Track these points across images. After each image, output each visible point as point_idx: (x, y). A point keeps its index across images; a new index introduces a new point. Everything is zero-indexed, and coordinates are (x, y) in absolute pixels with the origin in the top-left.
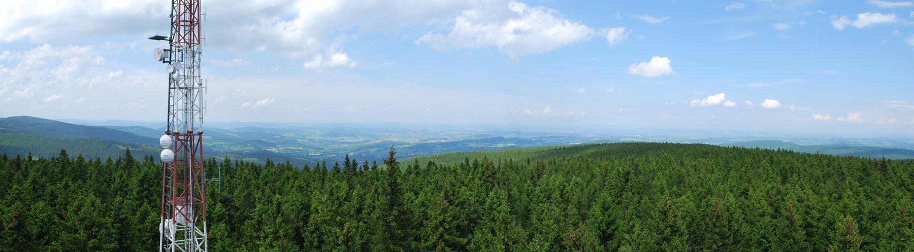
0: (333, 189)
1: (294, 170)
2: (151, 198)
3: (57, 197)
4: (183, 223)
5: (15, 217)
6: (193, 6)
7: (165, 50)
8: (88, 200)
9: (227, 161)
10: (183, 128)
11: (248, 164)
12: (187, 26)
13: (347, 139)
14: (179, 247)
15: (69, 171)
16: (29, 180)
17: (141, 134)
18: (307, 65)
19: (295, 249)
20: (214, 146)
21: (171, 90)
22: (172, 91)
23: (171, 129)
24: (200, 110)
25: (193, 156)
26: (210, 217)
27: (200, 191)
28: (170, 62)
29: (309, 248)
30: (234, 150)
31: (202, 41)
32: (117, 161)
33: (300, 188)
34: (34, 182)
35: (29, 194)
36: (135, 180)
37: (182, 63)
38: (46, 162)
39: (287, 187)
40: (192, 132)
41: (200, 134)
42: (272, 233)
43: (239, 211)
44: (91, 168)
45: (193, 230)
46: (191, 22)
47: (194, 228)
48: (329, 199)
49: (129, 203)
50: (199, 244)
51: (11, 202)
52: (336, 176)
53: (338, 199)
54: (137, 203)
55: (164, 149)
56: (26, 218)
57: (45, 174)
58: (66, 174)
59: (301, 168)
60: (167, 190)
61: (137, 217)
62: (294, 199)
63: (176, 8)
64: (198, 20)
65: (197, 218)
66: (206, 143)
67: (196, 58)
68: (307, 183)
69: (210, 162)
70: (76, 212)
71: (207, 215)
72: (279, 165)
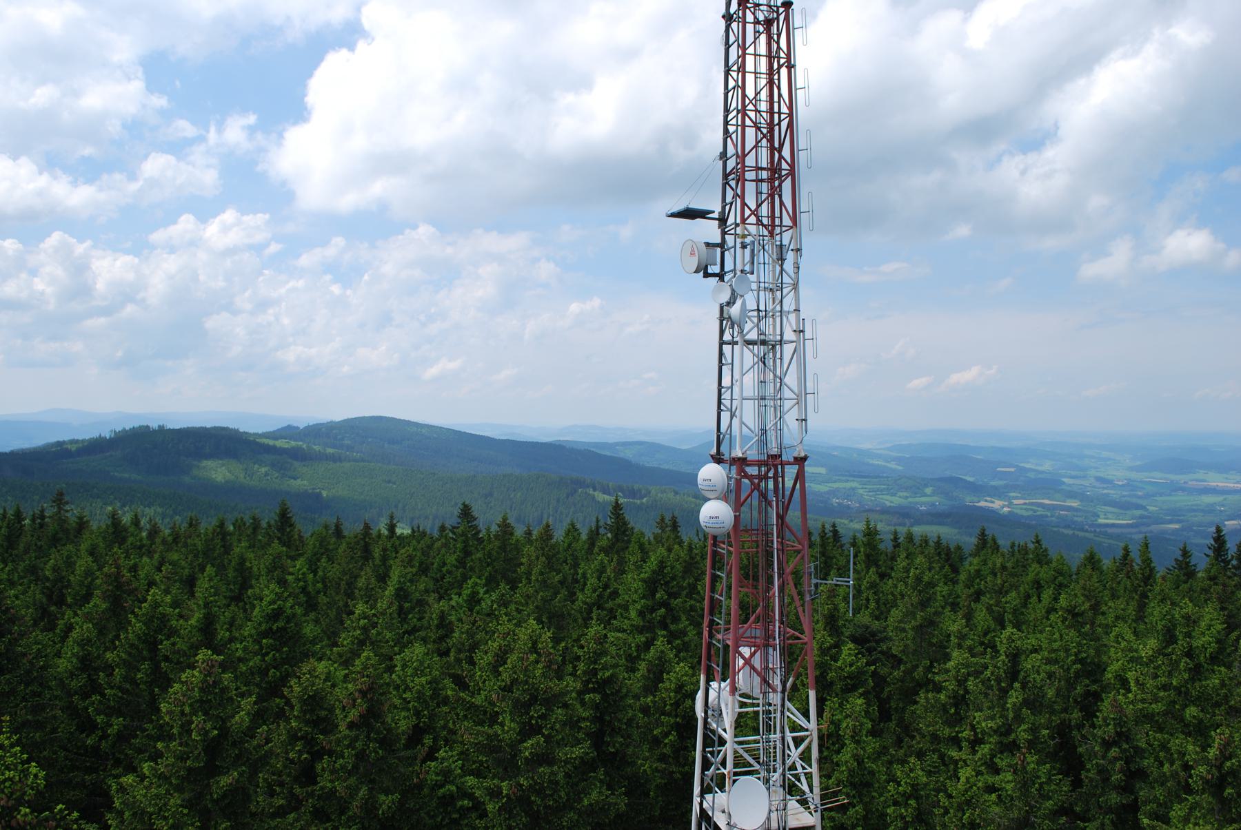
0: (1174, 626)
1: (1054, 564)
2: (673, 627)
3: (453, 631)
4: (756, 692)
5: (360, 691)
6: (777, 128)
7: (708, 245)
8: (523, 635)
9: (871, 533)
10: (755, 447)
11: (925, 541)
12: (762, 180)
13: (1216, 480)
14: (746, 756)
15: (480, 559)
16: (390, 591)
17: (649, 462)
18: (1092, 270)
19: (1057, 784)
20: (834, 493)
22: (727, 349)
23: (724, 448)
24: (801, 399)
25: (781, 517)
26: (825, 678)
27: (800, 609)
28: (721, 276)
29: (1096, 786)
30: (888, 504)
31: (804, 219)
32: (592, 531)
33: (1074, 614)
34: (401, 594)
35: (390, 627)
36: (633, 583)
37: (752, 278)
38: (426, 538)
39: (1036, 611)
40: (780, 456)
41: (800, 461)
42: (995, 732)
43: (902, 667)
44: (529, 550)
45: (783, 713)
46: (774, 170)
47: (783, 706)
48: (1160, 652)
49: (618, 639)
50: (796, 748)
51: (352, 651)
52: (1184, 587)
53: (1189, 654)
54: (641, 639)
56: (383, 694)
57: (424, 570)
58: (472, 569)
59: (1076, 558)
60: (715, 606)
61: (638, 674)
62: (1056, 645)
63: (734, 136)
64: (792, 165)
65: (791, 680)
66: (812, 485)
67: (789, 265)
68: (1093, 602)
69: (823, 535)
70: (495, 670)
71: (818, 673)
72: (1013, 545)
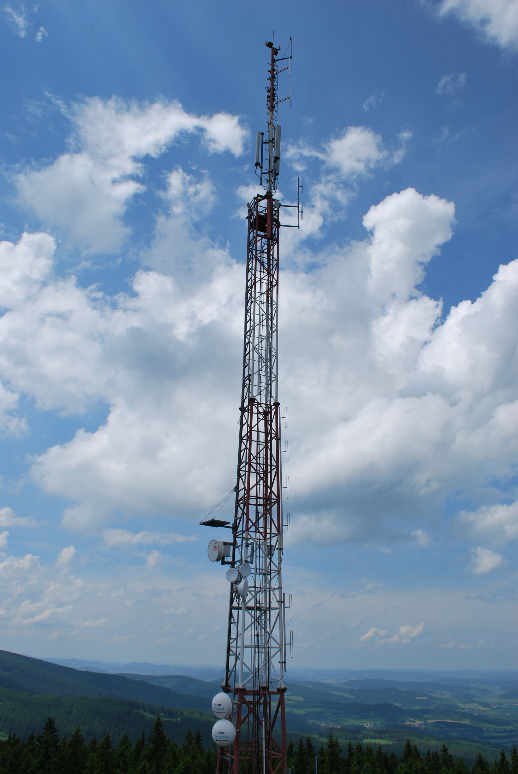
6: (269, 474)
7: (225, 543)
9: (333, 745)
10: (252, 680)
11: (370, 751)
12: (260, 505)
21: (233, 611)
22: (235, 612)
23: (231, 682)
24: (282, 648)
28: (232, 564)
37: (252, 566)
40: (268, 688)
41: (281, 691)
55: (220, 719)
63: (243, 477)
64: (278, 496)
67: (275, 559)
69: (301, 747)
